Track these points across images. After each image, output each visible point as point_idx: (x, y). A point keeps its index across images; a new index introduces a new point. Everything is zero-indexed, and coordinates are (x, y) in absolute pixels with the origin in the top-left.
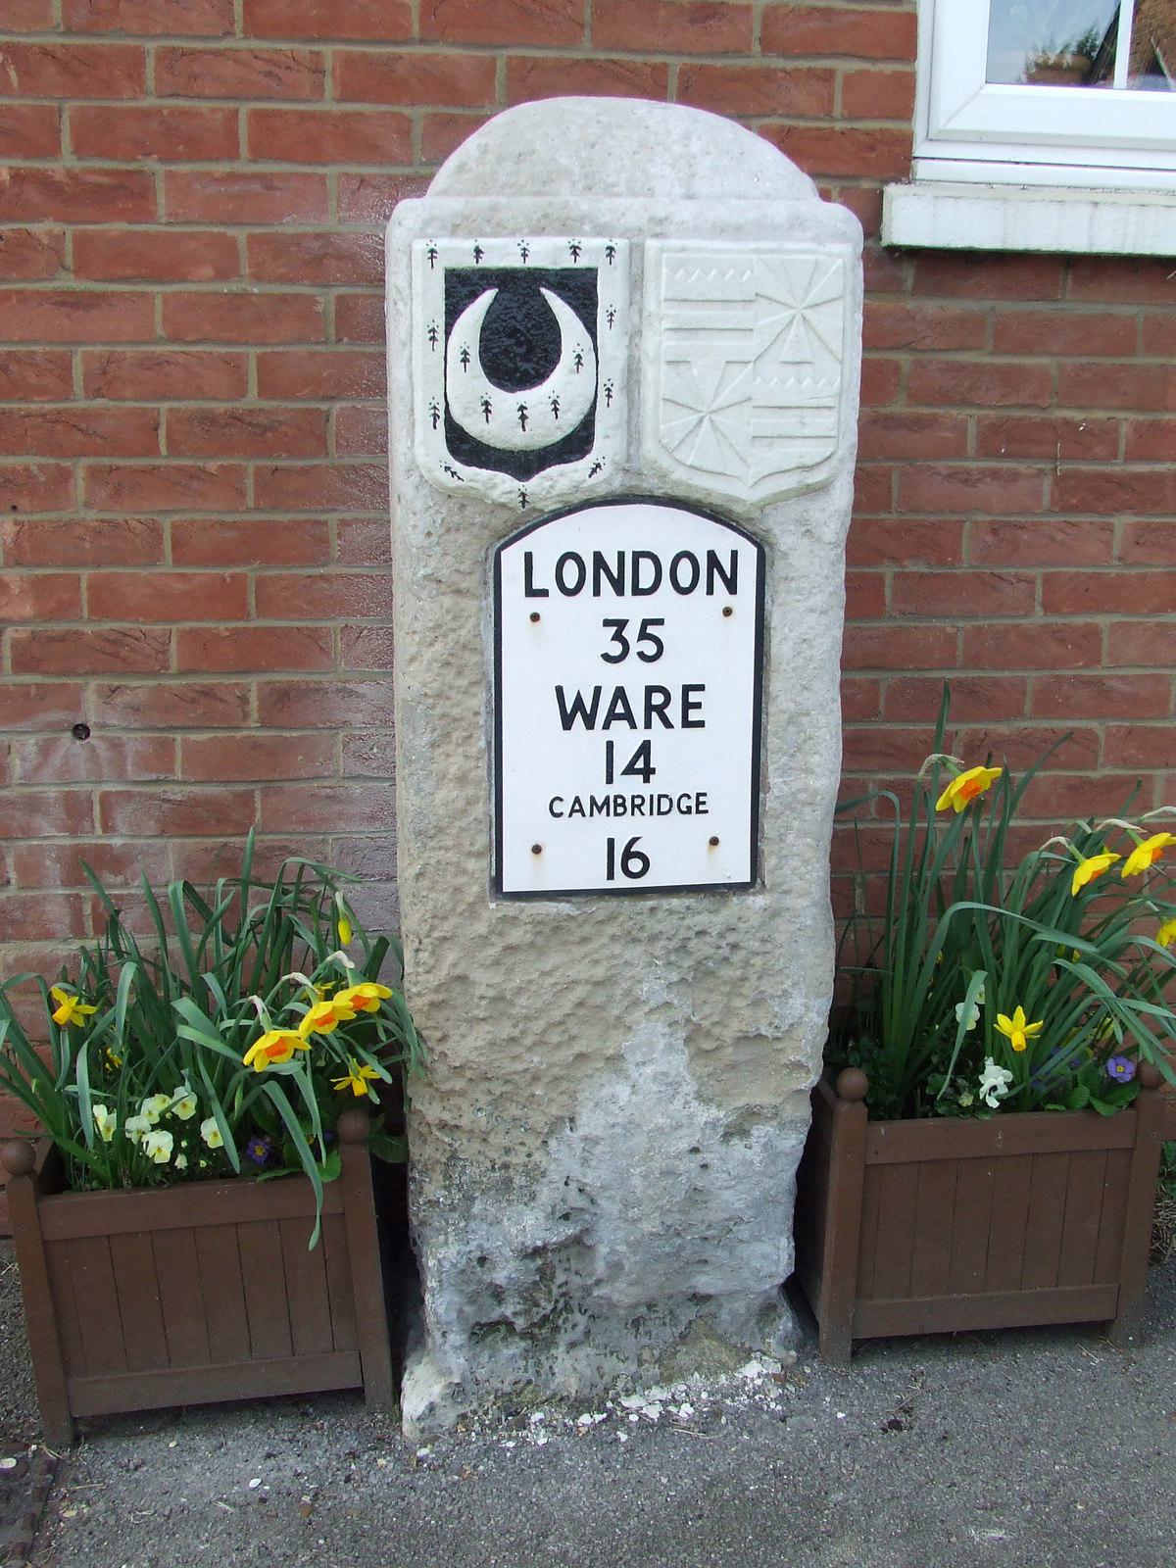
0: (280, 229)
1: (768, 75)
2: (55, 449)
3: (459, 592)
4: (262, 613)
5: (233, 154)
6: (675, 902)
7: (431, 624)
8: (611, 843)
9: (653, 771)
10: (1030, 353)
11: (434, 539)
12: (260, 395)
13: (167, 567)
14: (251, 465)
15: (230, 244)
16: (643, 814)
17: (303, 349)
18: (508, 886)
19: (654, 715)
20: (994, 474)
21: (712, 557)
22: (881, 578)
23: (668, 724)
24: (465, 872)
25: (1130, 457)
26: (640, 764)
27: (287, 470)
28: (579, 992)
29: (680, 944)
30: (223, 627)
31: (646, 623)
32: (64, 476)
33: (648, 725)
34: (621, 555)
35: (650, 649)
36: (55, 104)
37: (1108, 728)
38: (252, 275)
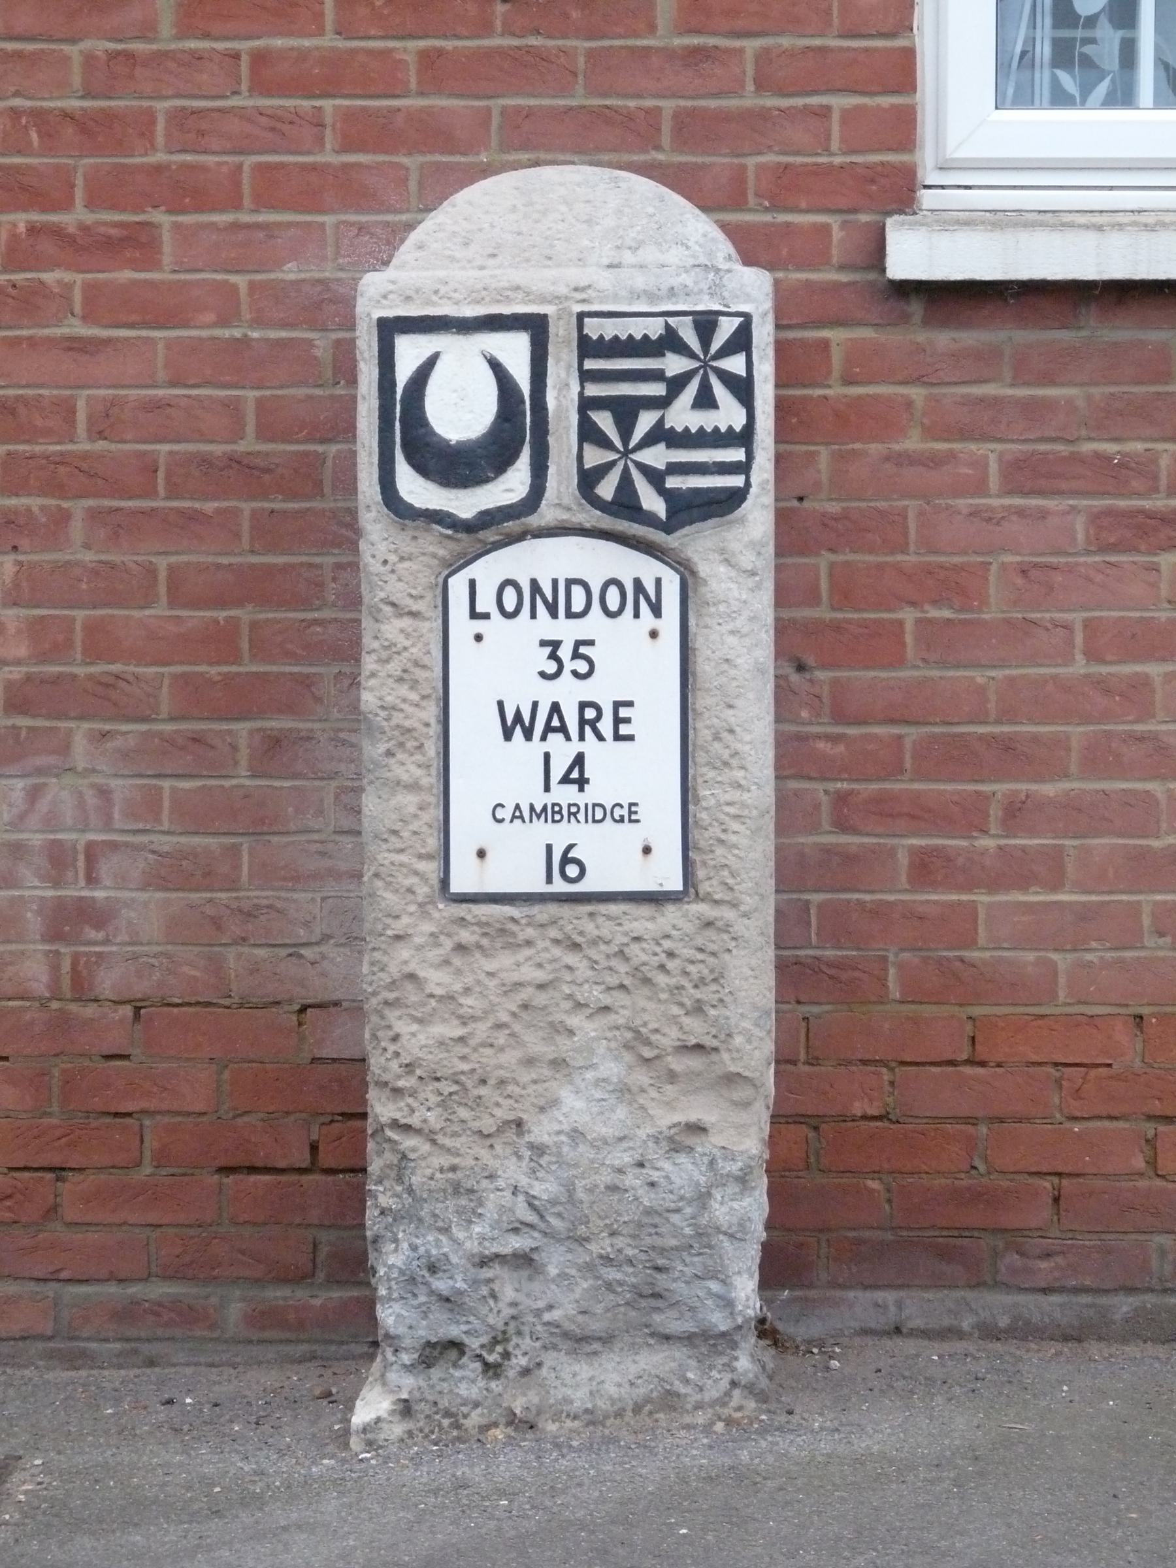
0: (280, 276)
1: (764, 115)
2: (57, 488)
3: (414, 615)
5: (237, 206)
6: (613, 909)
8: (549, 848)
9: (587, 781)
10: (1053, 383)
11: (388, 567)
13: (161, 609)
14: (247, 507)
15: (234, 288)
17: (302, 392)
18: (455, 888)
19: (588, 729)
20: (1021, 512)
21: (638, 585)
22: (900, 623)
23: (600, 738)
26: (575, 775)
27: (284, 512)
28: (524, 994)
29: (617, 949)
30: (214, 671)
31: (578, 644)
32: (64, 517)
33: (582, 737)
34: (555, 582)
35: (582, 667)
36: (70, 161)
37: (1169, 790)
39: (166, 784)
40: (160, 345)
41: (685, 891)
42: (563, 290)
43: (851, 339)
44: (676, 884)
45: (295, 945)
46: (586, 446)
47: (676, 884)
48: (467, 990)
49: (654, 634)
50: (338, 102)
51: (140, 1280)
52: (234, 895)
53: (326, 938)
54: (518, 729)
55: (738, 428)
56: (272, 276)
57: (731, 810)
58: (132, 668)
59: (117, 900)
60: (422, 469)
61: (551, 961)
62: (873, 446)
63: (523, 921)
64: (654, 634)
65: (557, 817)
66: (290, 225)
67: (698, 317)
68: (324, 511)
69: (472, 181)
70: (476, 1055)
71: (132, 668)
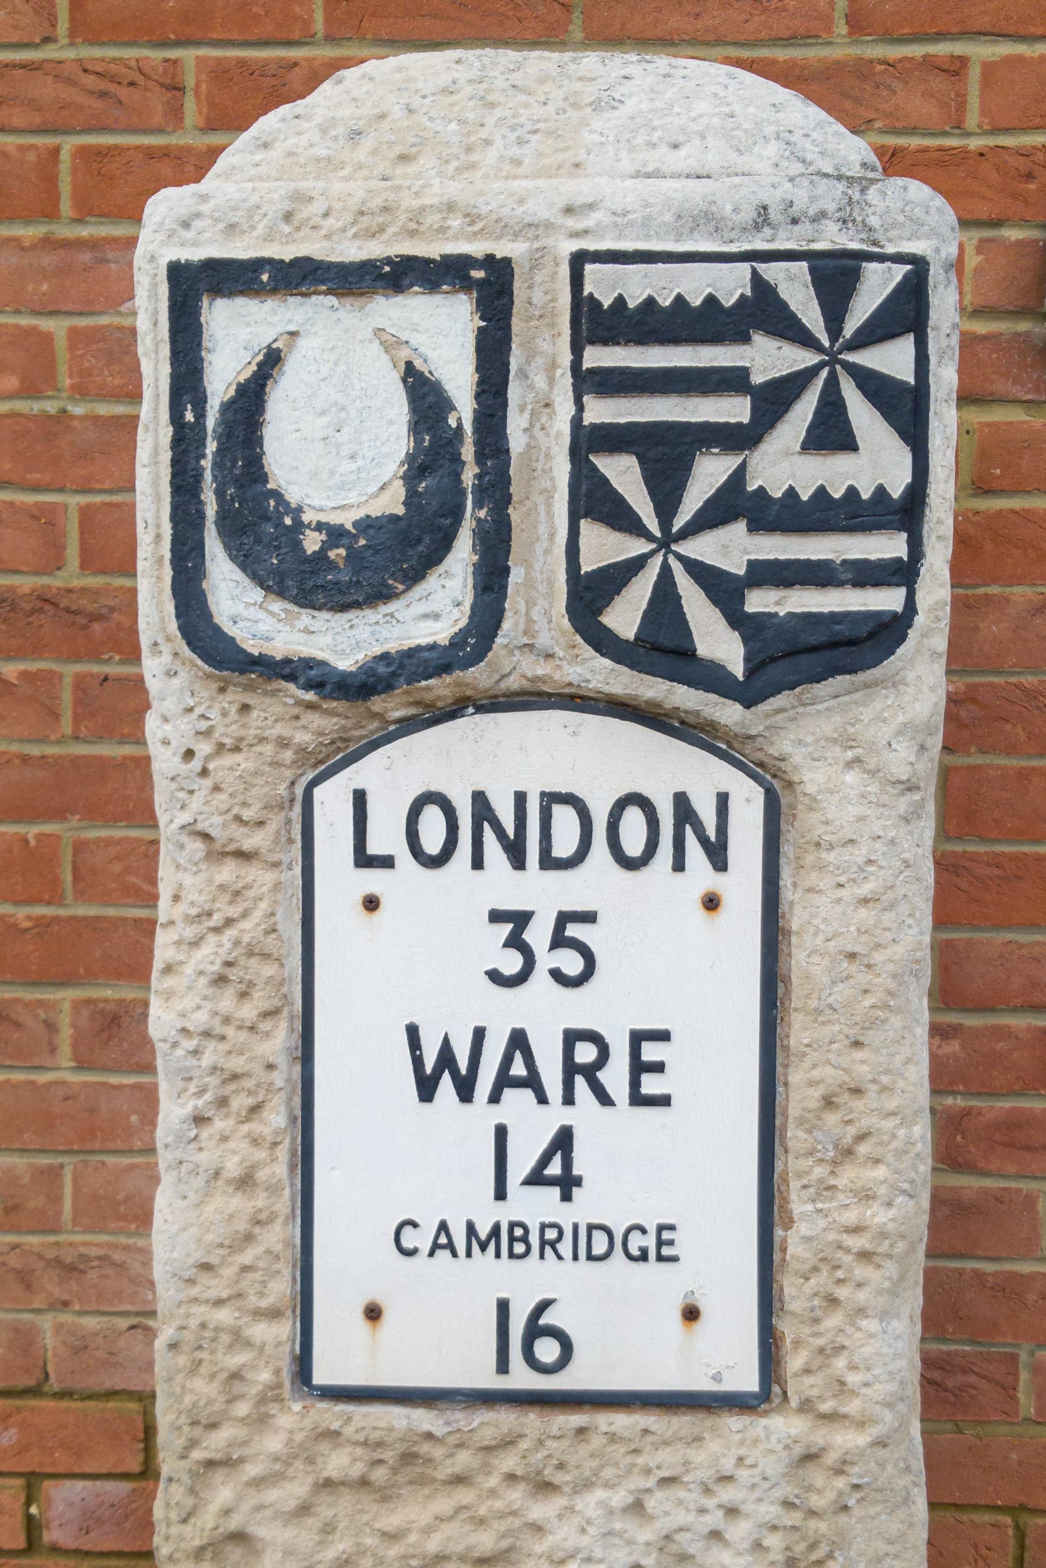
0: (116, 320)
3: (242, 855)
4: (81, 895)
5: (51, 214)
6: (621, 1421)
7: (194, 911)
8: (503, 1307)
9: (578, 1182)
12: (83, 566)
14: (70, 670)
15: (47, 338)
16: (560, 1257)
18: (320, 1377)
19: (580, 1081)
21: (682, 805)
23: (604, 1099)
24: (248, 1344)
26: (555, 1169)
30: (22, 913)
31: (564, 919)
33: (569, 1099)
34: (521, 799)
35: (572, 963)
38: (72, 386)
41: (765, 1394)
43: (989, 425)
44: (748, 1381)
45: (137, 1314)
46: (586, 526)
47: (748, 1381)
49: (711, 903)
50: (204, 52)
52: (52, 1239)
54: (446, 1080)
55: (896, 492)
56: (104, 320)
57: (857, 1242)
61: (502, 1516)
62: (1017, 590)
64: (711, 903)
65: (519, 1248)
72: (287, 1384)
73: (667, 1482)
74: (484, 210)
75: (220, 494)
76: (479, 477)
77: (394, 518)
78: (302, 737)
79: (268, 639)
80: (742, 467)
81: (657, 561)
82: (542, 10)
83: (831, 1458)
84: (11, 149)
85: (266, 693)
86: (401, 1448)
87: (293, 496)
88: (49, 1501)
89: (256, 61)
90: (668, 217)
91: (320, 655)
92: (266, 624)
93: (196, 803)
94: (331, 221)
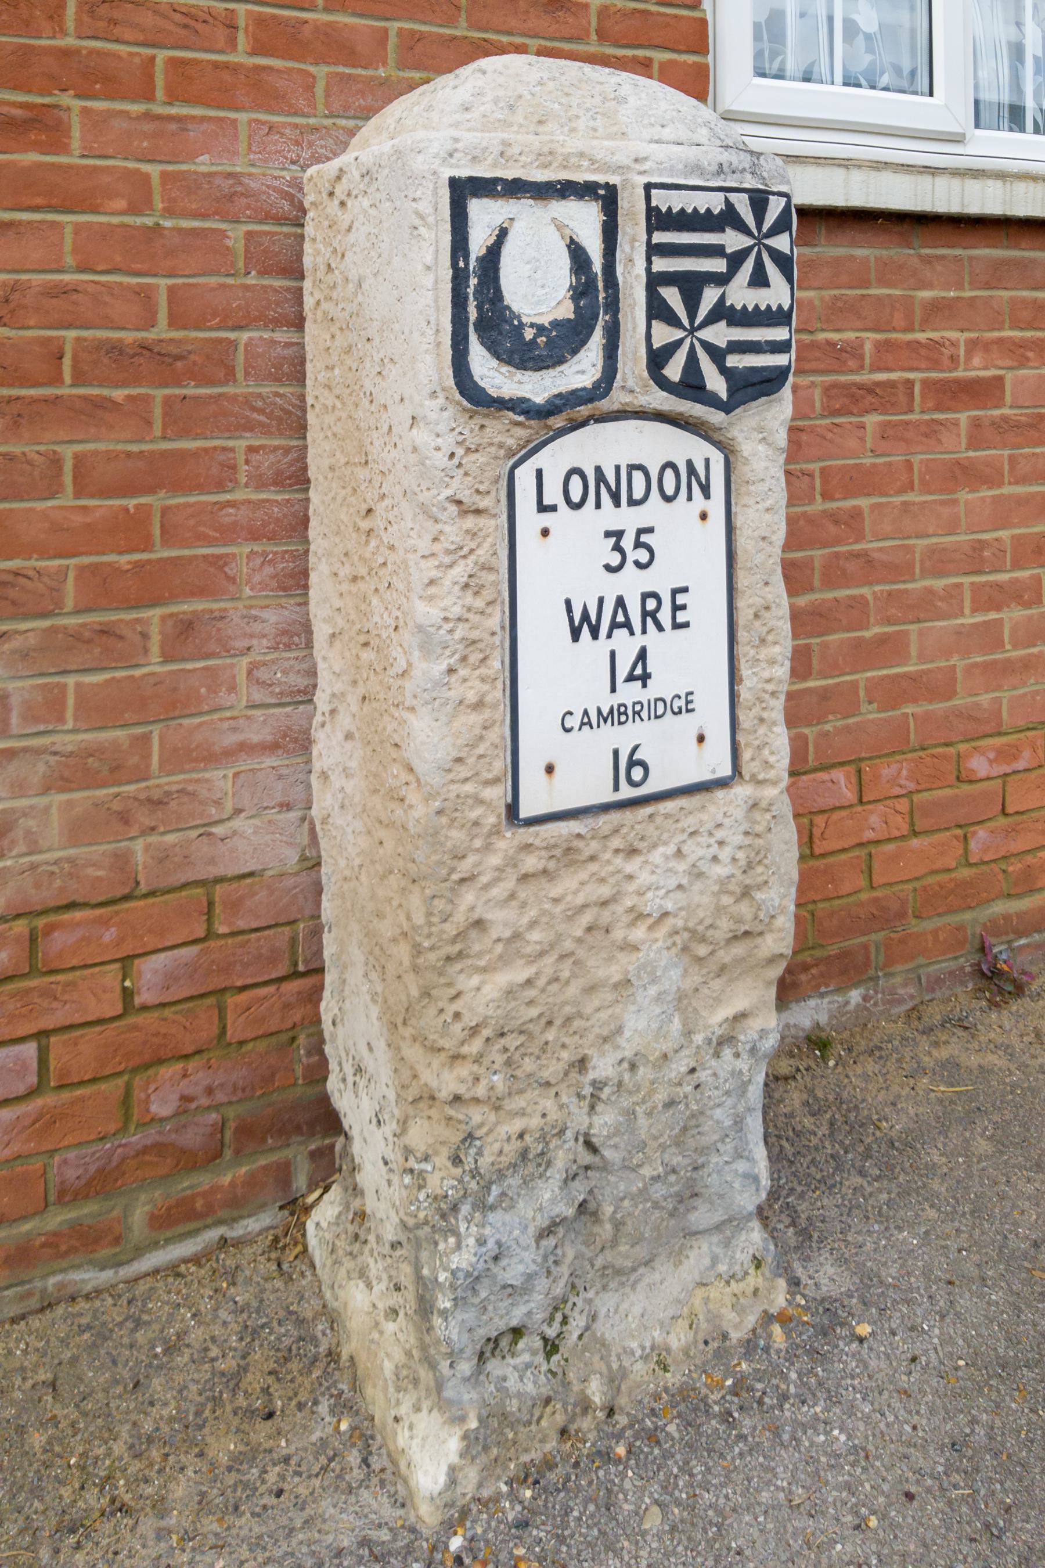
0: (193, 168)
3: (478, 512)
4: (166, 543)
5: (149, 96)
6: (669, 806)
7: (453, 547)
8: (616, 753)
9: (649, 676)
11: (456, 461)
13: (67, 499)
15: (146, 178)
17: (213, 280)
19: (649, 620)
23: (660, 628)
25: (875, 368)
27: (196, 398)
28: (586, 919)
30: (124, 560)
31: (640, 532)
33: (644, 631)
34: (618, 468)
35: (643, 556)
37: (874, 593)
39: (71, 681)
40: (68, 230)
42: (626, 161)
45: (205, 825)
46: (654, 322)
48: (533, 924)
49: (704, 516)
50: (250, 7)
51: (35, 1214)
52: (144, 784)
53: (238, 811)
55: (786, 308)
56: (184, 167)
58: (33, 563)
59: (13, 810)
60: (493, 348)
61: (613, 874)
63: (589, 836)
64: (704, 516)
66: (203, 119)
67: (754, 195)
68: (236, 396)
69: (487, 54)
70: (544, 996)
71: (33, 563)
72: (504, 822)
73: (693, 834)
74: (599, 157)
75: (479, 307)
76: (605, 298)
77: (569, 320)
78: (511, 442)
79: (500, 388)
80: (724, 294)
81: (688, 341)
82: (445, 8)
83: (763, 804)
84: (123, 54)
85: (494, 418)
86: (565, 846)
87: (515, 308)
88: (140, 972)
89: (283, 16)
90: (681, 166)
91: (527, 396)
92: (499, 380)
93: (455, 483)
94: (523, 158)
